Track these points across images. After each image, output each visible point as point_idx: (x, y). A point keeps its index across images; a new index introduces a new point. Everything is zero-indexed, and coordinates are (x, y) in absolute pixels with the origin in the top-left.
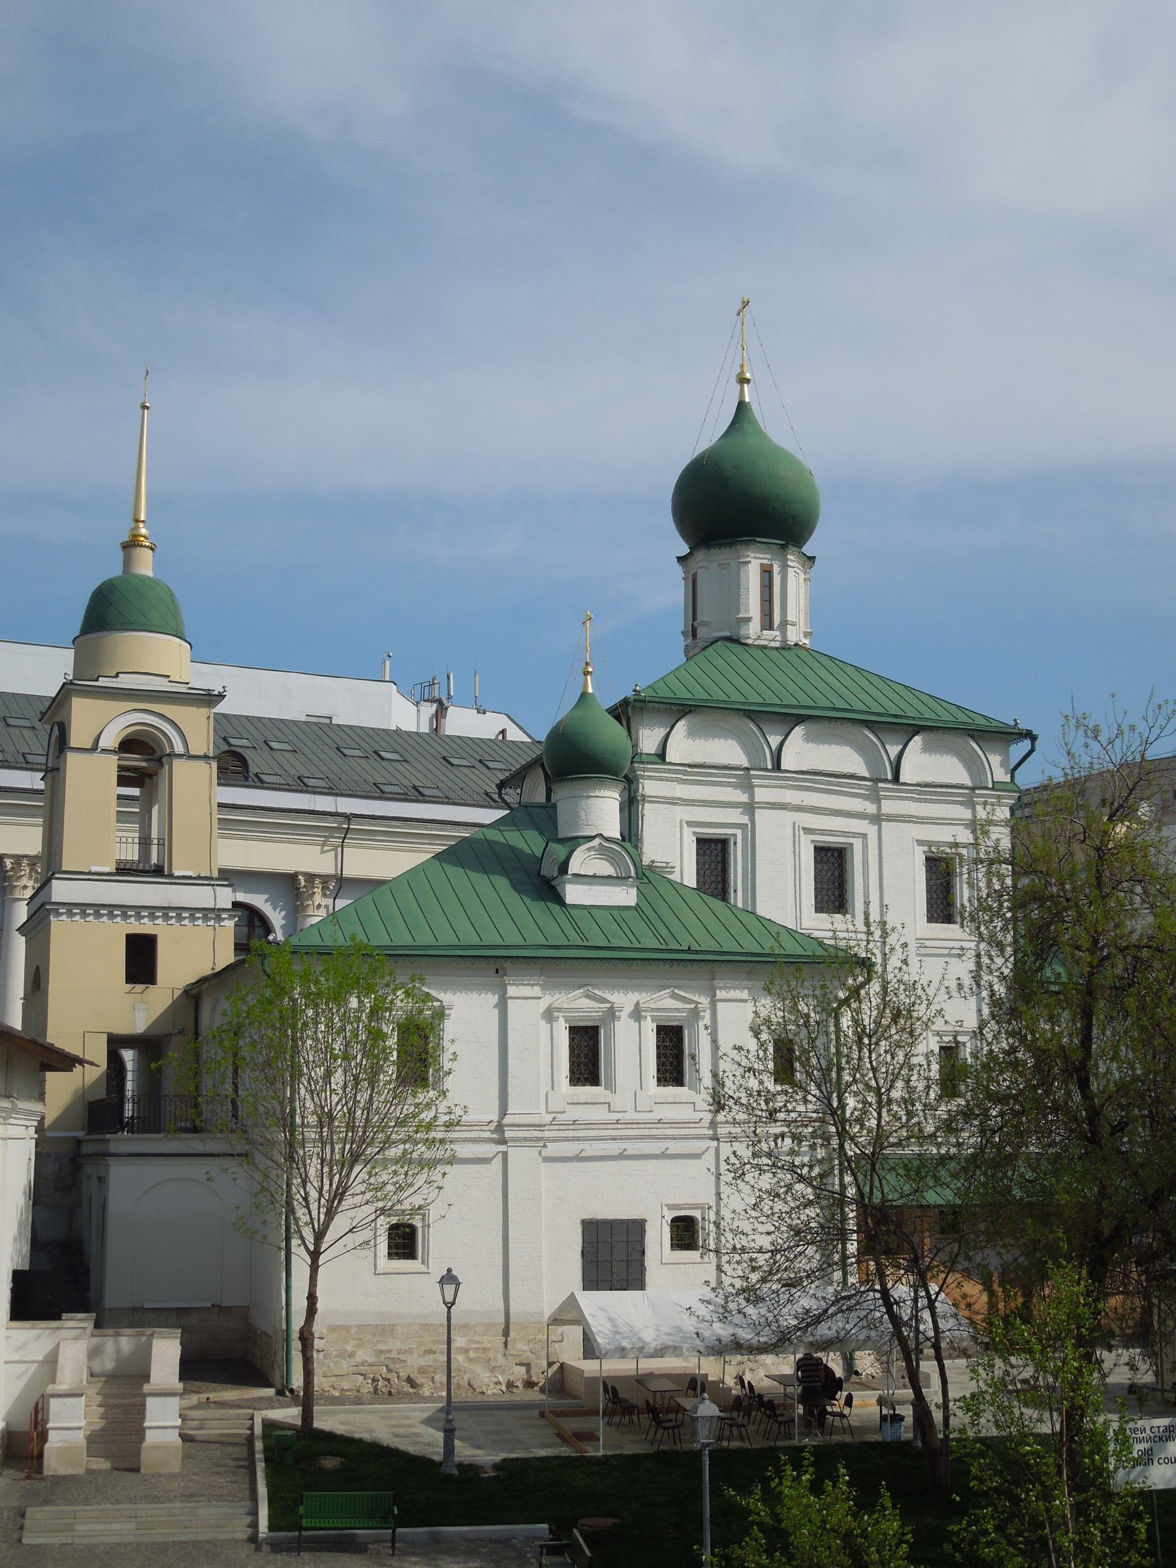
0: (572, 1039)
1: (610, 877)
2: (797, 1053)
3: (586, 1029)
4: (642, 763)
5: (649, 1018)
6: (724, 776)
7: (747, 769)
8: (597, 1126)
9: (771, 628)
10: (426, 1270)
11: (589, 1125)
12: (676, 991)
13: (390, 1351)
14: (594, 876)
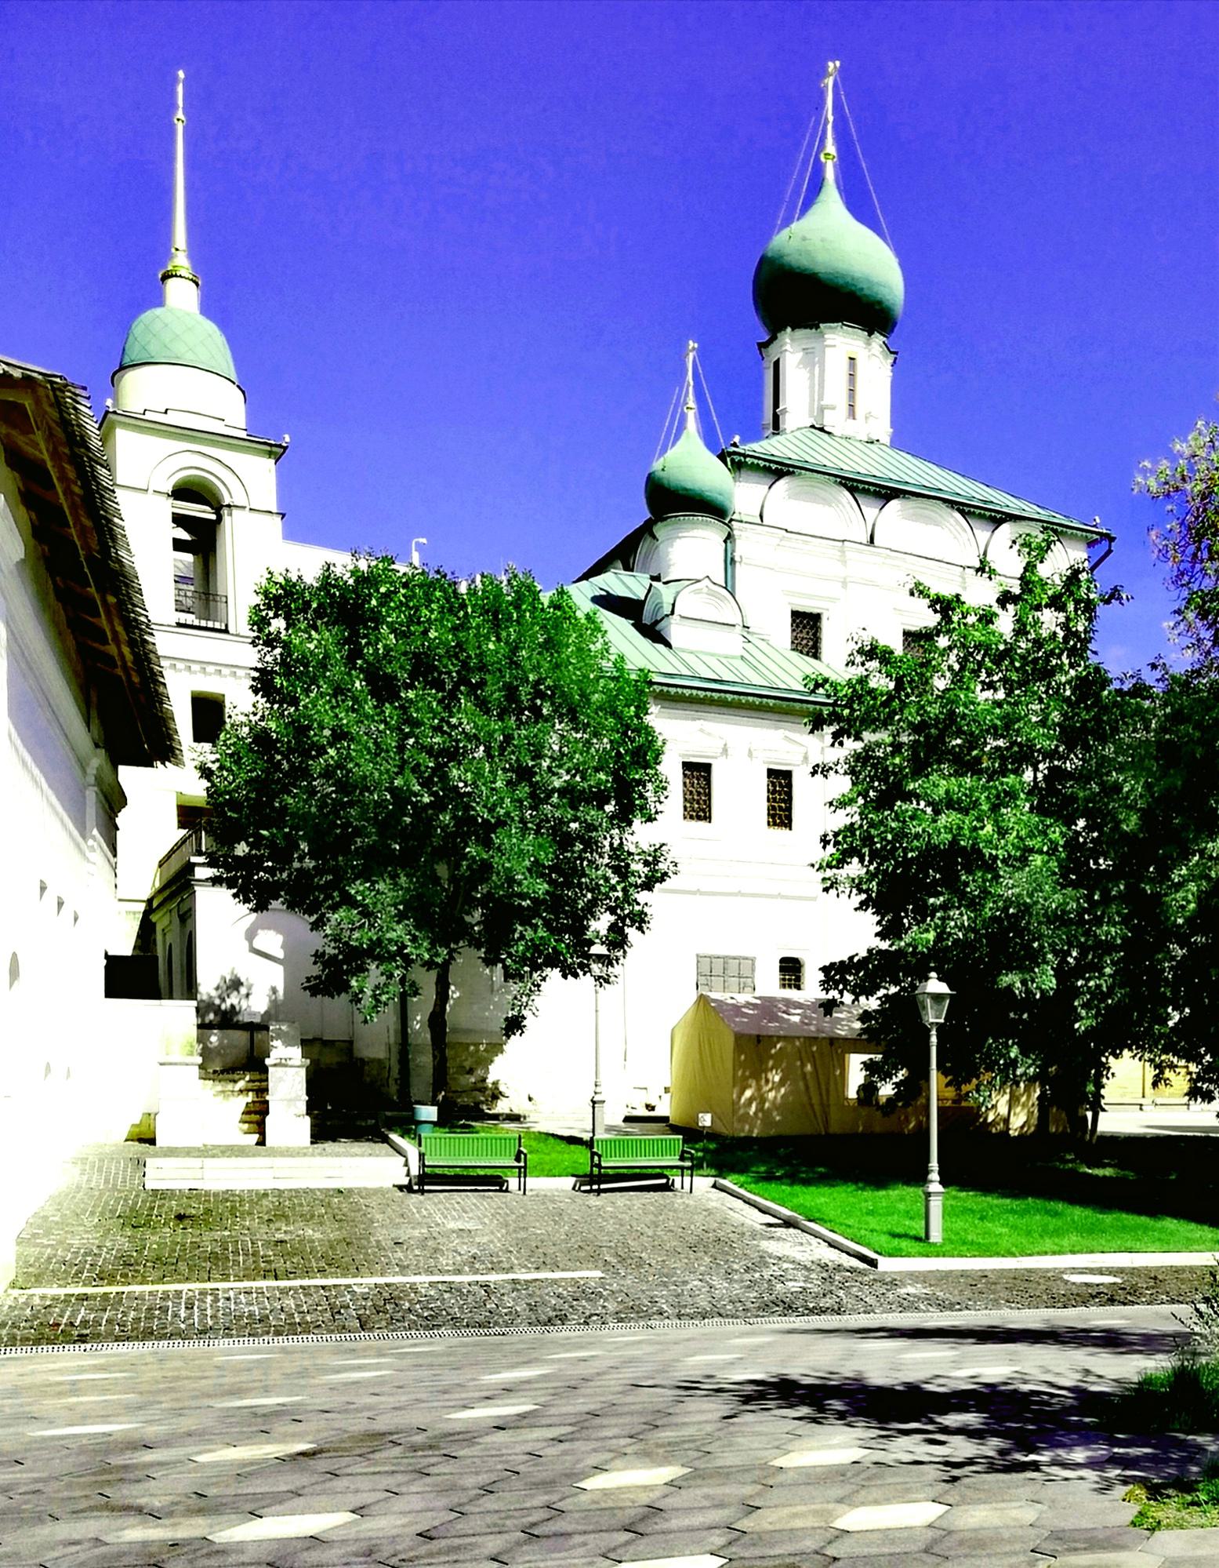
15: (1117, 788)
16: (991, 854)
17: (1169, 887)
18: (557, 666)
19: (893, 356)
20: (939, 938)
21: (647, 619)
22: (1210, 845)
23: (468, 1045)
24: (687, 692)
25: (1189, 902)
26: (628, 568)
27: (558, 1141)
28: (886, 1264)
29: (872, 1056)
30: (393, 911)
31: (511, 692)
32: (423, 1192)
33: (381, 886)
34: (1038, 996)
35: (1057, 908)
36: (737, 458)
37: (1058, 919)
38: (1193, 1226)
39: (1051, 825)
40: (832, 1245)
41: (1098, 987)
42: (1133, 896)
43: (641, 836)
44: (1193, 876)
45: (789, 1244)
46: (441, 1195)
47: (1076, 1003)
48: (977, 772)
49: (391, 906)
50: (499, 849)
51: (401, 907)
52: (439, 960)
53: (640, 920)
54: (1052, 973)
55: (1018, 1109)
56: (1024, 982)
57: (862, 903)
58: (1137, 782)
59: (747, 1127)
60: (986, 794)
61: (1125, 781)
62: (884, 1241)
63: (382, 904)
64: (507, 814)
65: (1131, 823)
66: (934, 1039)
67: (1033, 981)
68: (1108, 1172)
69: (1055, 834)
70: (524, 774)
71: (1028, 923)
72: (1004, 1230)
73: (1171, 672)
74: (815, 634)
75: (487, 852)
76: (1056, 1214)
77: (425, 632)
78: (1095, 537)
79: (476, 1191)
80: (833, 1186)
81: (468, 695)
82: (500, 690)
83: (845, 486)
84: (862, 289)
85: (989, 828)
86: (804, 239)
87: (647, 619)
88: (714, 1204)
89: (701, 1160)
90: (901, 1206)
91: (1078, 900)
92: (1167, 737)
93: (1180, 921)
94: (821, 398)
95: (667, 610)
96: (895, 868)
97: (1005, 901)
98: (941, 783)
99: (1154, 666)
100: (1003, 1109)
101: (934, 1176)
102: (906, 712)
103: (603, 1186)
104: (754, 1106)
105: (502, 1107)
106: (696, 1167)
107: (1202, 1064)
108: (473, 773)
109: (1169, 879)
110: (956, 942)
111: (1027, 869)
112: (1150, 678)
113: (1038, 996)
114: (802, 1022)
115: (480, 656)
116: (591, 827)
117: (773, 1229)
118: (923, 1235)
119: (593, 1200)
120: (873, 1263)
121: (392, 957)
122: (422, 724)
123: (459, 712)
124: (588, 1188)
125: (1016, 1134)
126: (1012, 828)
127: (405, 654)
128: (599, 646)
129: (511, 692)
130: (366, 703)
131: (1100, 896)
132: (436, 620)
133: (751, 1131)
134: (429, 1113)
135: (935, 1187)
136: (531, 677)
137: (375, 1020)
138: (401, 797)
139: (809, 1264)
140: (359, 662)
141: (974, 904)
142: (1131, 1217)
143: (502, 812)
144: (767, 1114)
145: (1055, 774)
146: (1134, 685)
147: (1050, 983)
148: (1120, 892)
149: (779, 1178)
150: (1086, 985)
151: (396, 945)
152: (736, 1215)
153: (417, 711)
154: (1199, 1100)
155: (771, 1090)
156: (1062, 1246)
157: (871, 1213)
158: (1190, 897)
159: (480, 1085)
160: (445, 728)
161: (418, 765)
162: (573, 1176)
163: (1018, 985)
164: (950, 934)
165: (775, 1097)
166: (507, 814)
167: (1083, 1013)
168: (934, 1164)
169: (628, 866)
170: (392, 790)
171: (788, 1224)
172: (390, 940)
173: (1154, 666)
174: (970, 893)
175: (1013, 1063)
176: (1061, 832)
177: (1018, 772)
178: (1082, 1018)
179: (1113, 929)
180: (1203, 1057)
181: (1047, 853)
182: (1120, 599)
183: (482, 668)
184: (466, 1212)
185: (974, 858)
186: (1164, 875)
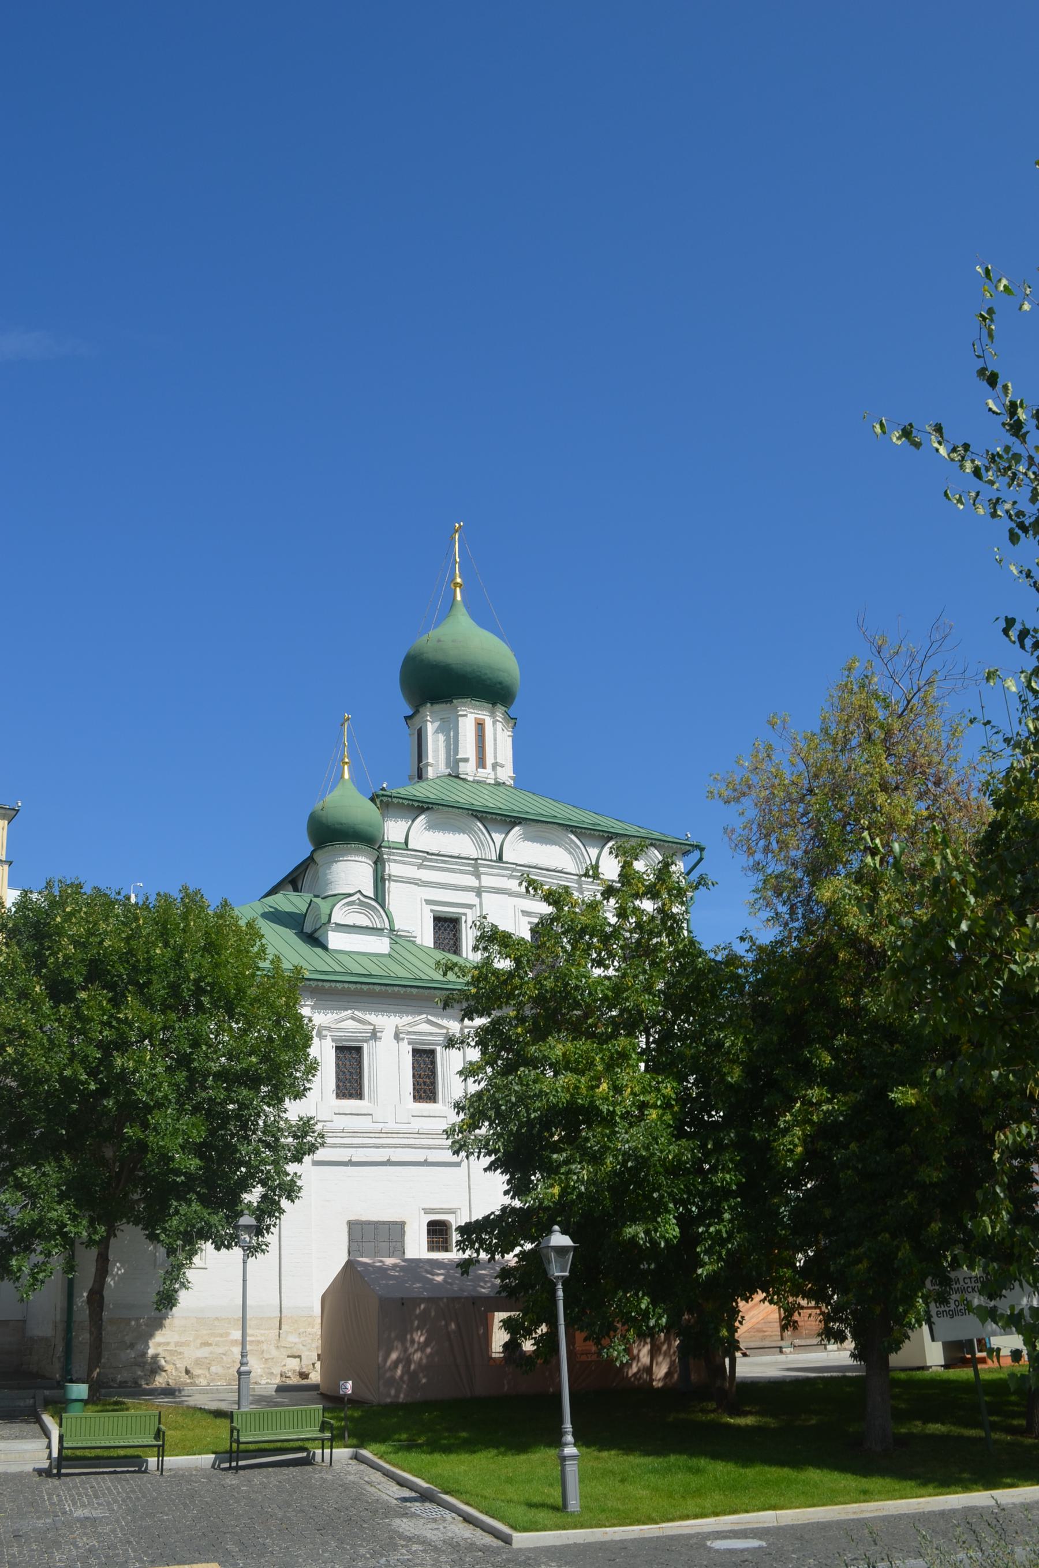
0: (337, 1058)
1: (367, 928)
2: (422, 1306)
3: (350, 1049)
4: (389, 848)
5: (406, 1041)
6: (457, 864)
7: (476, 859)
8: (361, 1135)
9: (484, 767)
10: (203, 1266)
11: (355, 1133)
12: (429, 1017)
13: (168, 1344)
14: (354, 926)
15: (719, 1044)
16: (608, 1110)
17: (777, 1133)
18: (217, 966)
19: (514, 721)
20: (564, 1192)
21: (308, 929)
22: (810, 1092)
23: (130, 1320)
24: (339, 986)
25: (796, 1146)
26: (296, 890)
27: (205, 1415)
28: (522, 1540)
29: (512, 1313)
30: (56, 1191)
31: (174, 988)
32: (59, 1475)
33: (47, 1169)
34: (663, 1245)
35: (673, 1159)
36: (385, 799)
37: (675, 1169)
38: (836, 1475)
39: (662, 1082)
40: (468, 1519)
41: (719, 1232)
42: (744, 1144)
43: (294, 1110)
44: (797, 1121)
45: (422, 1521)
46: (77, 1479)
47: (698, 1250)
48: (591, 1036)
49: (55, 1187)
50: (155, 1129)
51: (64, 1188)
52: (97, 1237)
53: (291, 1191)
54: (674, 1221)
55: (660, 1359)
56: (647, 1232)
57: (492, 1163)
58: (737, 1038)
59: (393, 1392)
60: (600, 1056)
61: (725, 1037)
62: (520, 1512)
63: (46, 1185)
64: (166, 1097)
65: (734, 1076)
66: (560, 1293)
67: (656, 1231)
68: (749, 1421)
69: (668, 1089)
70: (184, 1061)
71: (647, 1175)
72: (645, 1493)
73: (758, 942)
74: (454, 935)
75: (143, 1132)
76: (697, 1471)
77: (101, 943)
78: (688, 848)
79: (115, 1472)
80: (474, 1452)
81: (134, 994)
82: (164, 988)
83: (476, 817)
84: (486, 674)
85: (604, 1086)
86: (439, 641)
87: (308, 929)
88: (351, 1478)
89: (342, 1429)
90: (541, 1471)
91: (692, 1150)
92: (760, 999)
93: (790, 1164)
94: (456, 752)
95: (324, 919)
96: (520, 1127)
97: (623, 1155)
98: (558, 1047)
99: (742, 939)
100: (645, 1358)
101: (569, 1438)
102: (525, 987)
103: (241, 1463)
104: (400, 1367)
105: (160, 1381)
106: (337, 1438)
107: (830, 1304)
108: (135, 1060)
109: (776, 1125)
110: (580, 1195)
111: (642, 1123)
112: (740, 949)
113: (663, 1245)
114: (445, 1280)
115: (149, 960)
116: (242, 1106)
117: (408, 1504)
118: (561, 1504)
119: (231, 1479)
120: (507, 1540)
121: (52, 1236)
122: (92, 1020)
123: (126, 1009)
124: (227, 1465)
125: (660, 1384)
126: (626, 1085)
127: (82, 961)
128: (255, 949)
129: (174, 988)
130: (44, 1004)
131: (714, 1145)
132: (111, 932)
133: (397, 1396)
134: (80, 1390)
135: (570, 1450)
136: (192, 976)
137: (31, 1298)
138: (69, 1085)
139: (440, 1544)
140: (44, 971)
141: (596, 1159)
142: (773, 1469)
143: (161, 1095)
144: (413, 1376)
145: (666, 1036)
146: (727, 956)
147: (673, 1231)
148: (731, 1140)
149: (419, 1446)
150: (707, 1231)
151: (56, 1224)
152: (372, 1490)
153: (88, 1008)
154: (832, 1341)
155: (416, 1351)
156: (704, 1508)
157: (510, 1481)
158: (796, 1141)
159: (140, 1360)
160: (114, 1023)
161: (87, 1056)
162: (213, 1453)
163: (642, 1235)
164: (574, 1188)
165: (421, 1359)
166: (166, 1097)
167: (706, 1259)
168: (568, 1426)
169: (277, 1140)
170: (63, 1080)
171: (425, 1497)
172: (51, 1220)
173: (742, 939)
174: (591, 1148)
175: (645, 1315)
176: (673, 1088)
177: (631, 1034)
178: (705, 1264)
179: (728, 1176)
180: (831, 1297)
181: (661, 1107)
182: (706, 885)
183: (149, 970)
184: (97, 1498)
185: (591, 1114)
186: (773, 1122)
